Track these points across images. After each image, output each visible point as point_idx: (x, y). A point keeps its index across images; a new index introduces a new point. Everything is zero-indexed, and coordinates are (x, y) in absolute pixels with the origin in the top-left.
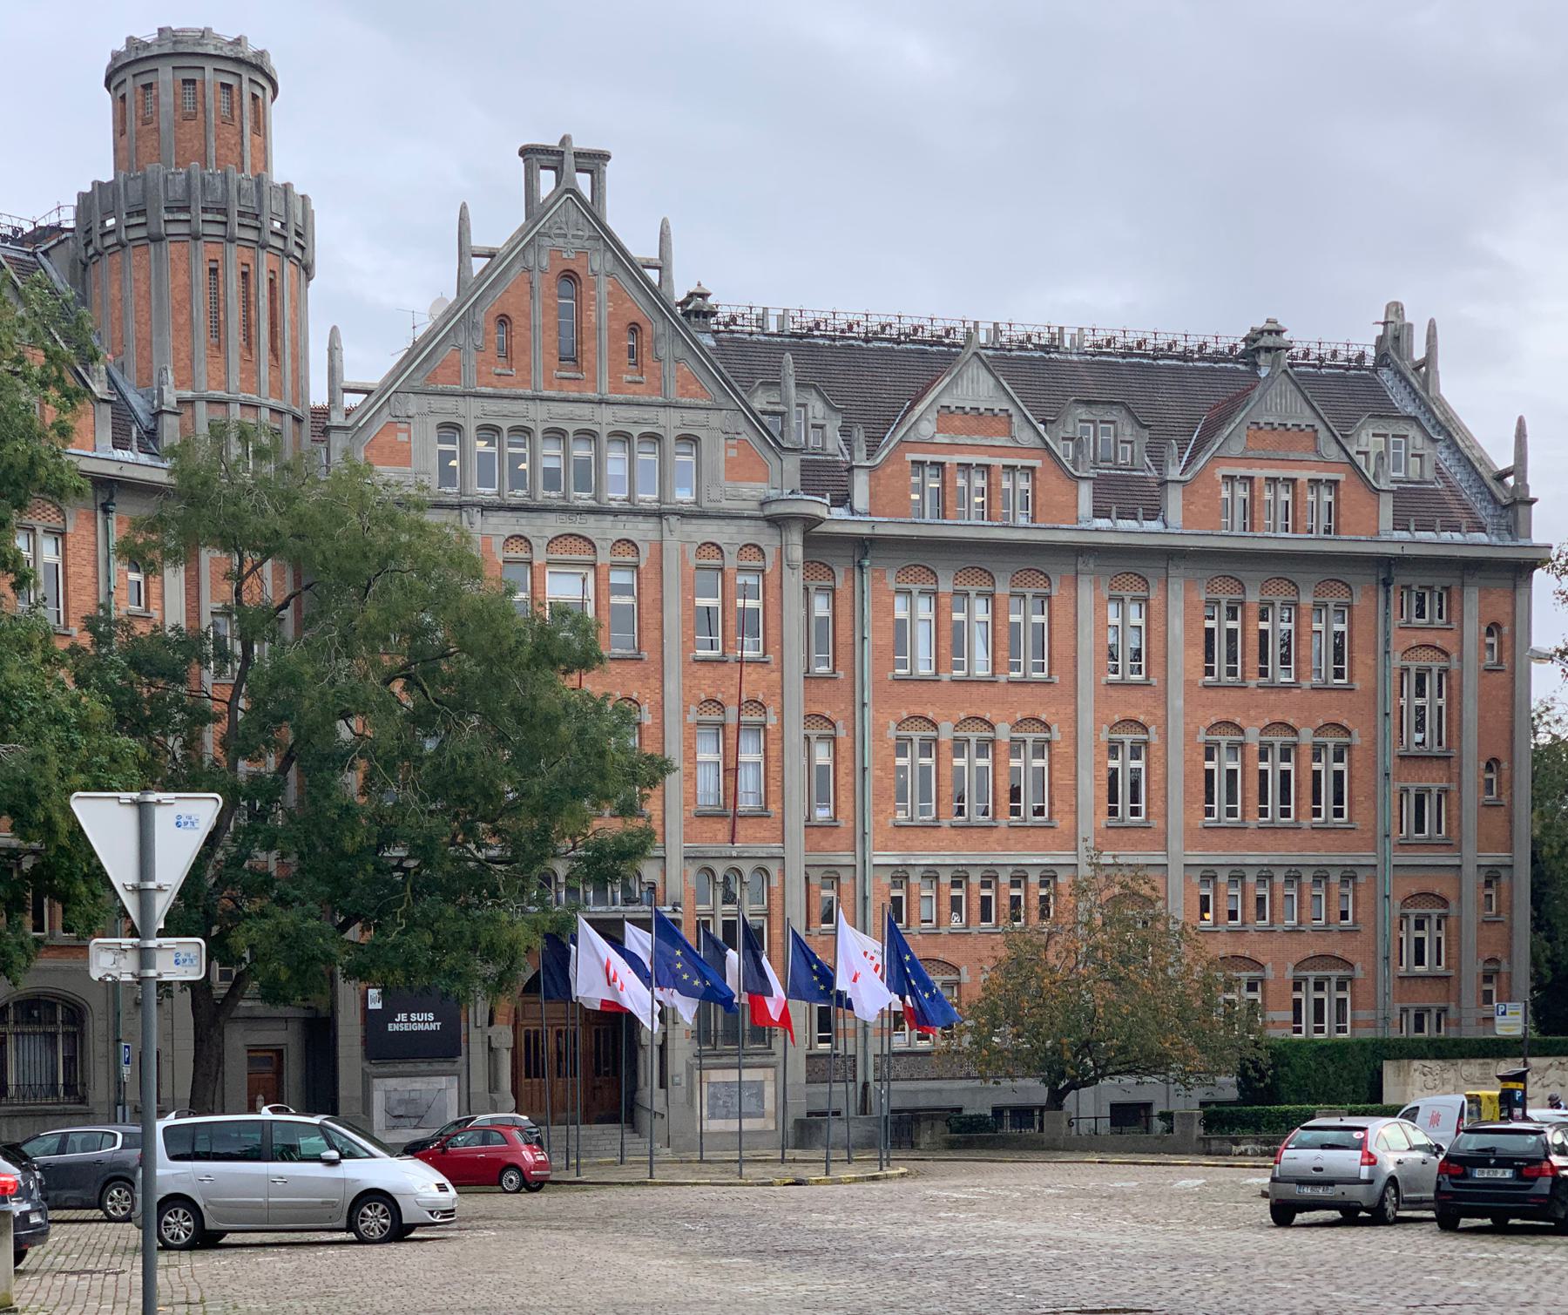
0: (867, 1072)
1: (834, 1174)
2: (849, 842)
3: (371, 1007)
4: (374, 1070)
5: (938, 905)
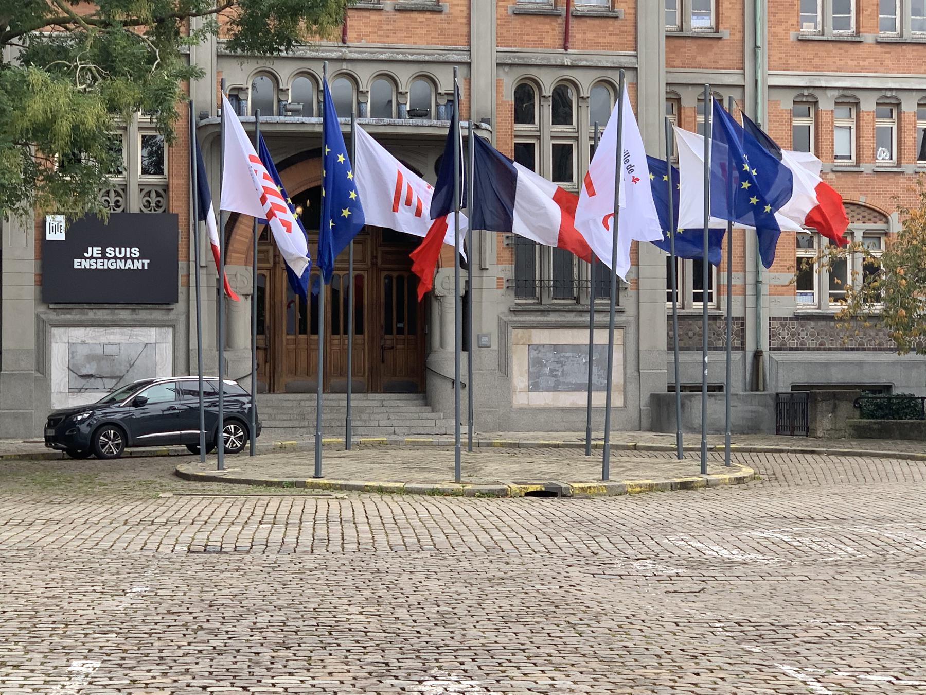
0: (759, 337)
1: (617, 478)
2: (736, 57)
3: (49, 237)
4: (53, 316)
5: (858, 138)
